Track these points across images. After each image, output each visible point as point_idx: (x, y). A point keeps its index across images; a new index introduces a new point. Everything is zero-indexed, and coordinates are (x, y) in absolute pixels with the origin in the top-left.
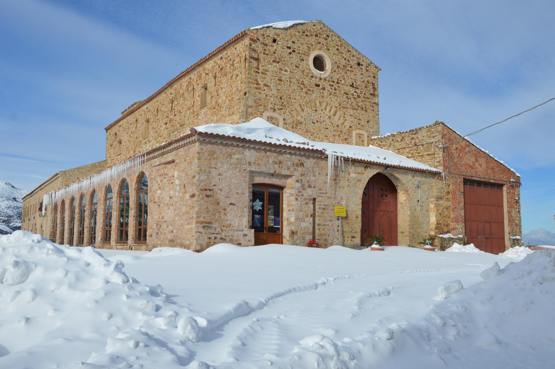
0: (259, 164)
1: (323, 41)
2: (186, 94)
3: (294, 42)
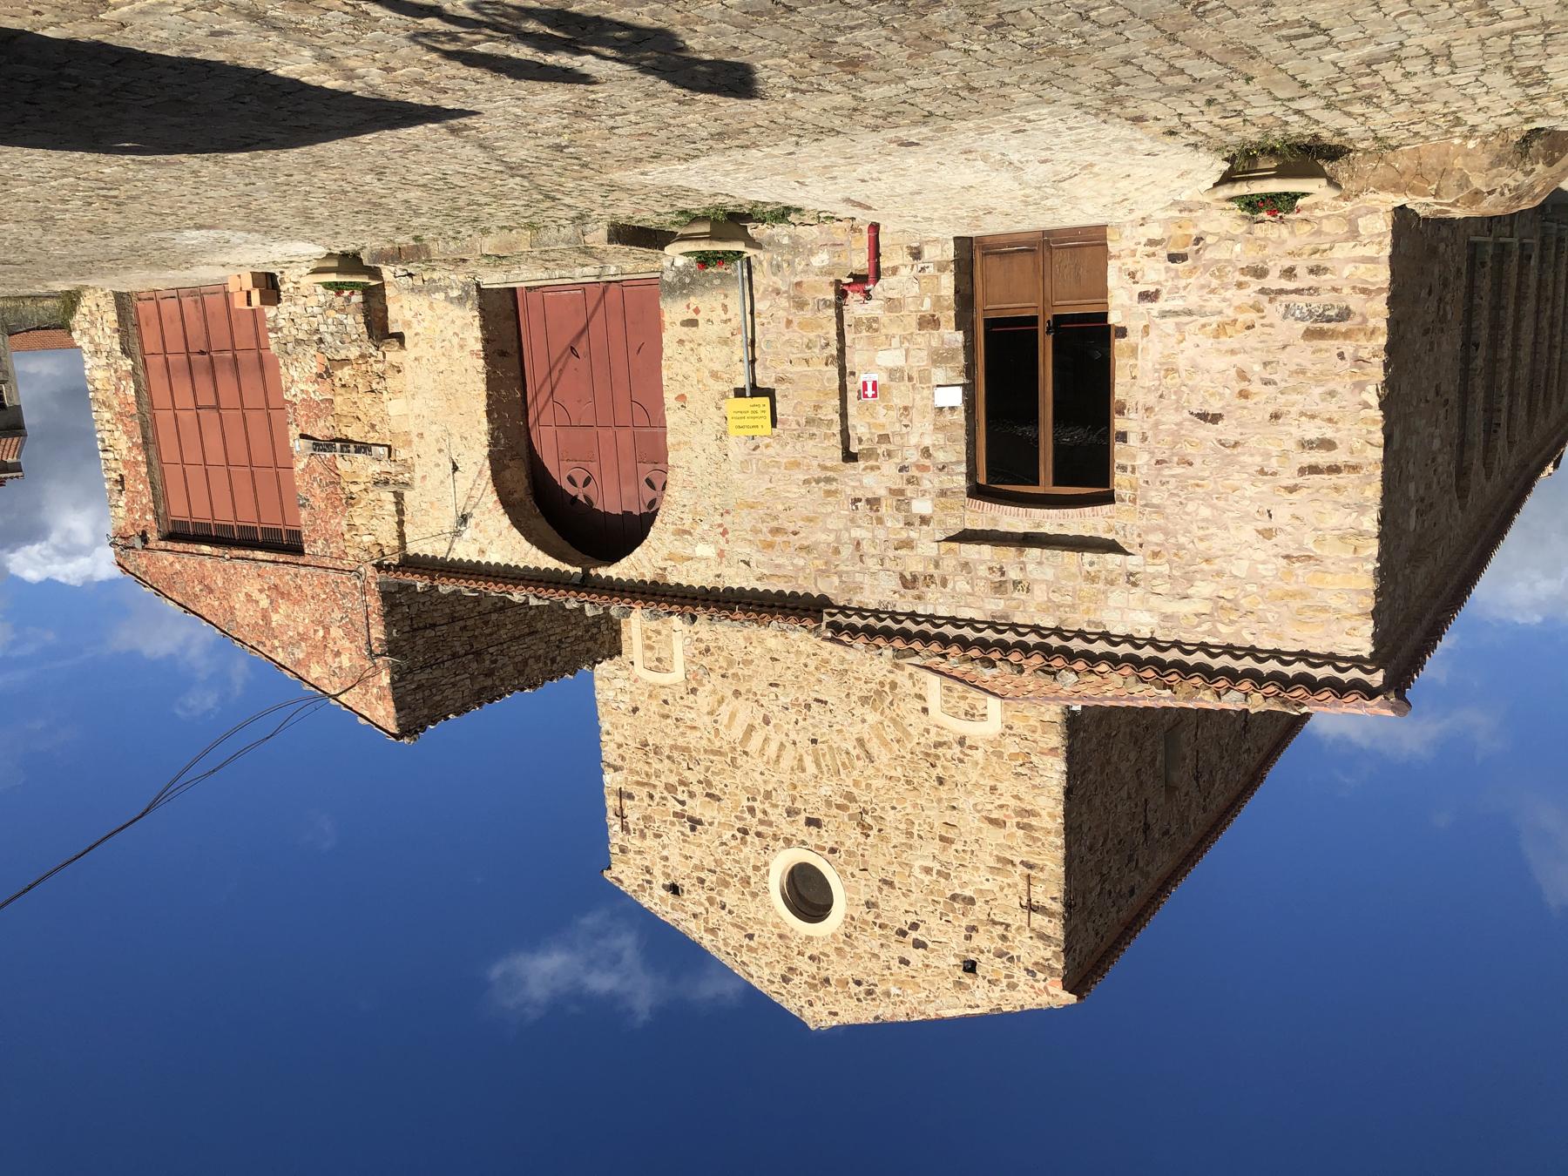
1: (803, 964)
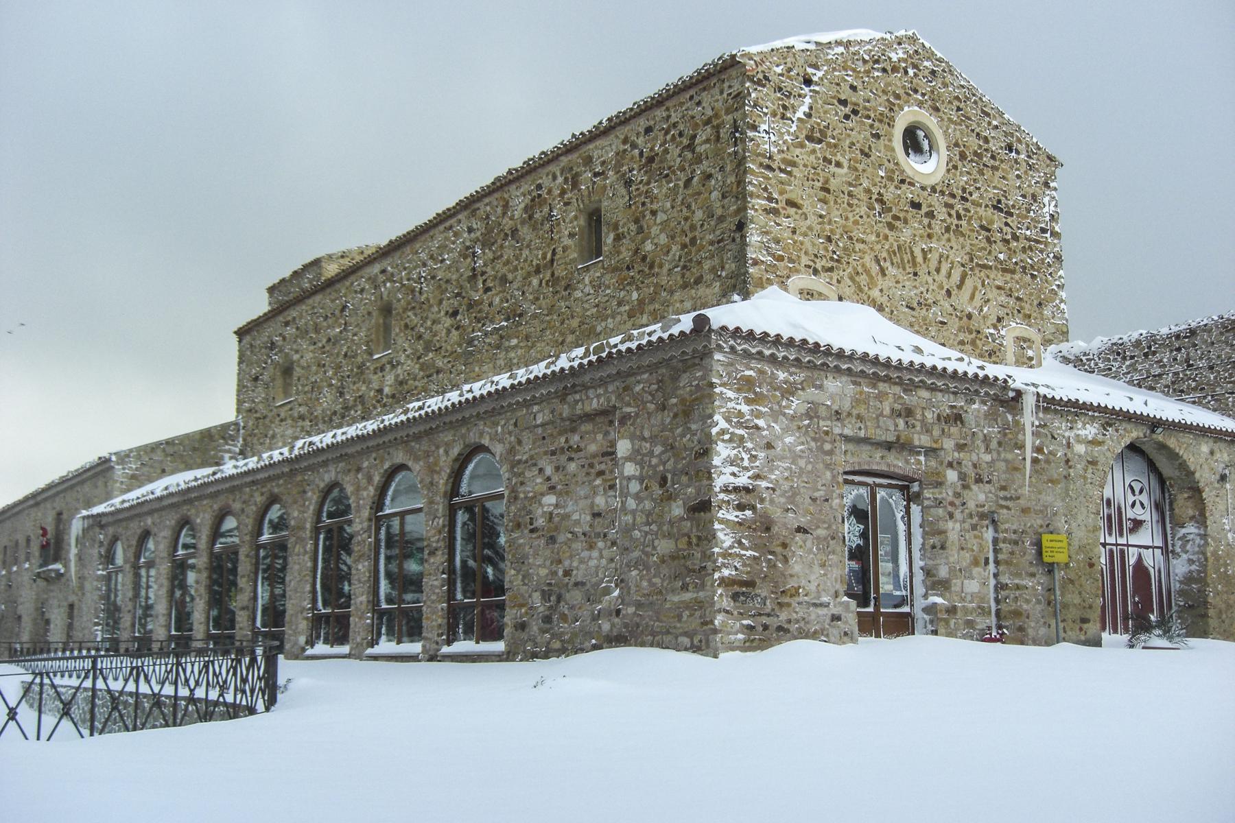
0: (859, 417)
2: (525, 231)
3: (853, 88)
